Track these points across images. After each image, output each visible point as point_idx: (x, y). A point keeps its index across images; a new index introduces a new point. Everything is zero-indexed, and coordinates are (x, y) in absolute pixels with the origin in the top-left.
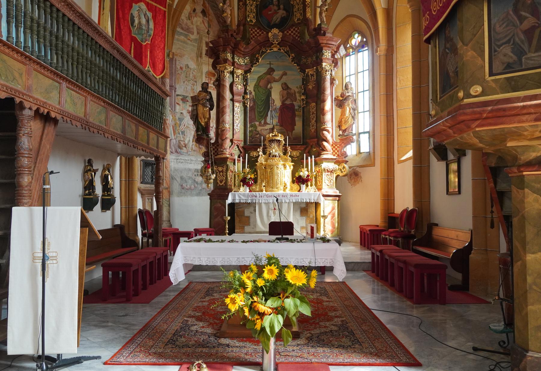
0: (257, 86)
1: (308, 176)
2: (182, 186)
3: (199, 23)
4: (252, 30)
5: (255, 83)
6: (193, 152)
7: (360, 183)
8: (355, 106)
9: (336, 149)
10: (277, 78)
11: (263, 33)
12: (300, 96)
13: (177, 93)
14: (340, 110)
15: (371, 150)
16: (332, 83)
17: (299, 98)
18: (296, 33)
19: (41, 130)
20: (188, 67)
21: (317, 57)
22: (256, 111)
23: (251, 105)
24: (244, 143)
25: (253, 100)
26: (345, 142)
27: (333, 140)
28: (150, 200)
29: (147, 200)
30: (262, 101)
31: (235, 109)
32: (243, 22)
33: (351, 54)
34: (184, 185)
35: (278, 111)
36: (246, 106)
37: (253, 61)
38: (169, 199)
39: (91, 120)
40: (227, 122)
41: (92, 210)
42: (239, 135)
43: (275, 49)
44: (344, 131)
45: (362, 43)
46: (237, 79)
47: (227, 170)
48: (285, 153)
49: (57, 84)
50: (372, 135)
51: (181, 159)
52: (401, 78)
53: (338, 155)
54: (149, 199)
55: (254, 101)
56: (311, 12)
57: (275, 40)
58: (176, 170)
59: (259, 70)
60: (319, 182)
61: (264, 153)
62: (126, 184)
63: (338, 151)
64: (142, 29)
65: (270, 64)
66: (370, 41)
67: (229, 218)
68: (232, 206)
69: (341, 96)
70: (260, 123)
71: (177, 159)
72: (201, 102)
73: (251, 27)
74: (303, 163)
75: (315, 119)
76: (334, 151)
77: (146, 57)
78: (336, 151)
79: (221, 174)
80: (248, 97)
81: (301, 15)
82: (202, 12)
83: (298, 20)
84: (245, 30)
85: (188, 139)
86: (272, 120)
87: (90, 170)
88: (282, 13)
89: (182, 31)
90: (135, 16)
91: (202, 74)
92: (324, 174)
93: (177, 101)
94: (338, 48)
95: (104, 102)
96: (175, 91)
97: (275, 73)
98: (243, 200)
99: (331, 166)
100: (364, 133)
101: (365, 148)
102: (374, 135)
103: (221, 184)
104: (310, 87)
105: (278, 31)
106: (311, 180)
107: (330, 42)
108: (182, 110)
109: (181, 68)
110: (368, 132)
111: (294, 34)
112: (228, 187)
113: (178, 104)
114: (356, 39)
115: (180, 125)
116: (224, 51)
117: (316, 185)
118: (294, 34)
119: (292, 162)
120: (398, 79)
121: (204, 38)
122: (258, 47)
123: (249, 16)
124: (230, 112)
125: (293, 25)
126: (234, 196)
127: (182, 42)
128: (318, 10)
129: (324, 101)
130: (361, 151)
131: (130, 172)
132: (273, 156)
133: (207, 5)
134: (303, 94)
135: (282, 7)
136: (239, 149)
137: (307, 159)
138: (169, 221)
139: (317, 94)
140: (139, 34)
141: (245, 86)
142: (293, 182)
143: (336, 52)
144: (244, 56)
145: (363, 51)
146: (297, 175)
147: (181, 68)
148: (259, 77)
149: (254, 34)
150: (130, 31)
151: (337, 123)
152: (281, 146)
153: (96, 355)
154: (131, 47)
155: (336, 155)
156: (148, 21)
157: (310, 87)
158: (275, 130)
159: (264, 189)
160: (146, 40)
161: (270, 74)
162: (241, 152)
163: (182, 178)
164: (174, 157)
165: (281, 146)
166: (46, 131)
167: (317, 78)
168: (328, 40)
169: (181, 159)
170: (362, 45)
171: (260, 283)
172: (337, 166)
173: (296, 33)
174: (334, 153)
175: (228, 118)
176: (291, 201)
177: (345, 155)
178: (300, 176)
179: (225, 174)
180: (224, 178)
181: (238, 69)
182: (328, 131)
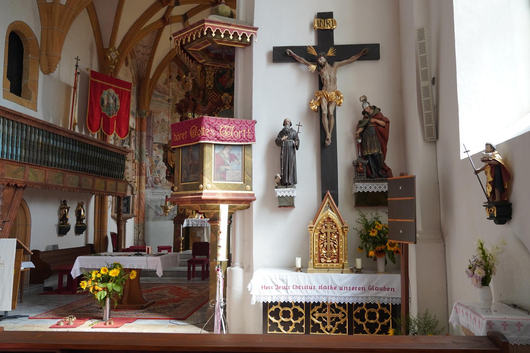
2: (156, 213)
3: (174, 86)
13: (154, 141)
19: (13, 193)
34: (159, 212)
39: (49, 182)
41: (65, 234)
49: (22, 168)
58: (151, 201)
62: (99, 214)
64: (110, 107)
67: (183, 238)
68: (187, 228)
77: (113, 125)
82: (176, 78)
85: (163, 176)
87: (64, 208)
89: (159, 94)
93: (154, 148)
95: (61, 170)
96: (152, 140)
108: (158, 154)
109: (158, 122)
112: (186, 214)
116: (186, 111)
121: (178, 98)
126: (188, 221)
133: (182, 72)
138: (144, 240)
147: (158, 122)
150: (101, 109)
153: (26, 315)
154: (100, 123)
156: (115, 101)
160: (113, 114)
163: (156, 207)
164: (150, 191)
166: (16, 193)
171: (99, 276)
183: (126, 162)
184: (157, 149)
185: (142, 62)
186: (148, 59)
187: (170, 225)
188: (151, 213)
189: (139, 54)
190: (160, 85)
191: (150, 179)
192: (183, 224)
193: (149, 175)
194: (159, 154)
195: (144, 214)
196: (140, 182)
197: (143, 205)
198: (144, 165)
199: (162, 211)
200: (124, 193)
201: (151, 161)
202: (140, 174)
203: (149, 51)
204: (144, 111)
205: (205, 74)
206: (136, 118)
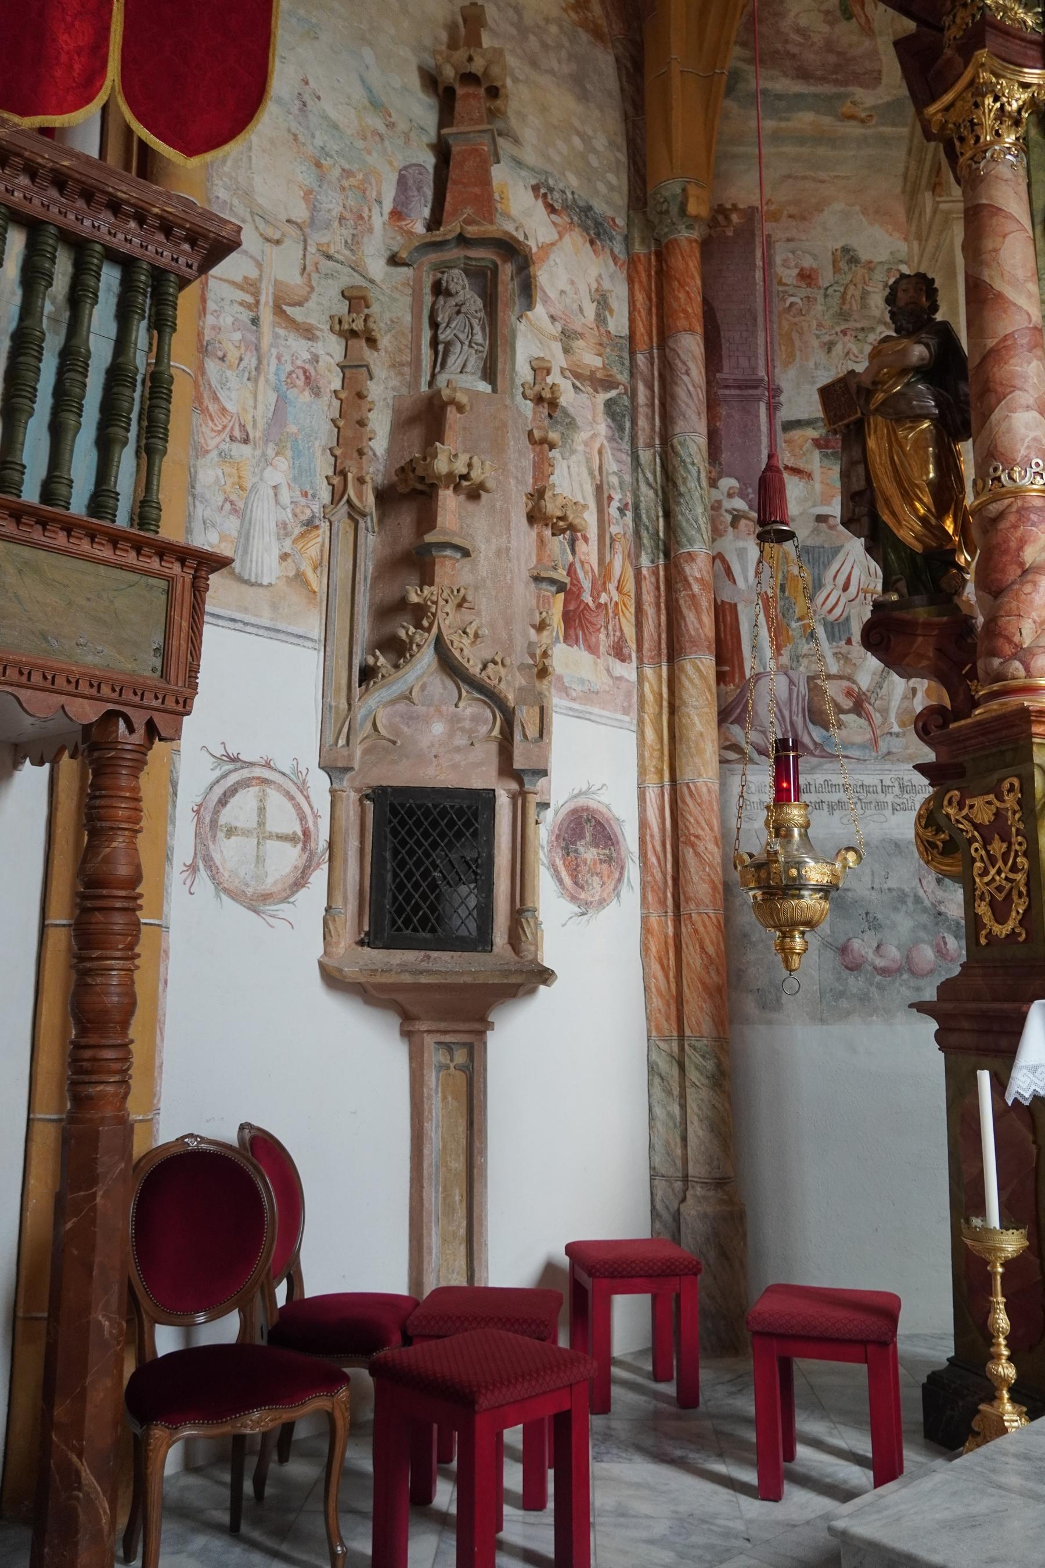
2: (844, 950)
13: (785, 414)
20: (854, 260)
28: (460, 1057)
29: (434, 1056)
34: (863, 946)
51: (829, 786)
54: (449, 1047)
79: (998, 847)
96: (773, 408)
103: (1002, 931)
109: (807, 277)
113: (796, 471)
115: (818, 585)
127: (801, 140)
169: (829, 786)
187: (917, 1051)
190: (802, 32)
206: (632, 263)
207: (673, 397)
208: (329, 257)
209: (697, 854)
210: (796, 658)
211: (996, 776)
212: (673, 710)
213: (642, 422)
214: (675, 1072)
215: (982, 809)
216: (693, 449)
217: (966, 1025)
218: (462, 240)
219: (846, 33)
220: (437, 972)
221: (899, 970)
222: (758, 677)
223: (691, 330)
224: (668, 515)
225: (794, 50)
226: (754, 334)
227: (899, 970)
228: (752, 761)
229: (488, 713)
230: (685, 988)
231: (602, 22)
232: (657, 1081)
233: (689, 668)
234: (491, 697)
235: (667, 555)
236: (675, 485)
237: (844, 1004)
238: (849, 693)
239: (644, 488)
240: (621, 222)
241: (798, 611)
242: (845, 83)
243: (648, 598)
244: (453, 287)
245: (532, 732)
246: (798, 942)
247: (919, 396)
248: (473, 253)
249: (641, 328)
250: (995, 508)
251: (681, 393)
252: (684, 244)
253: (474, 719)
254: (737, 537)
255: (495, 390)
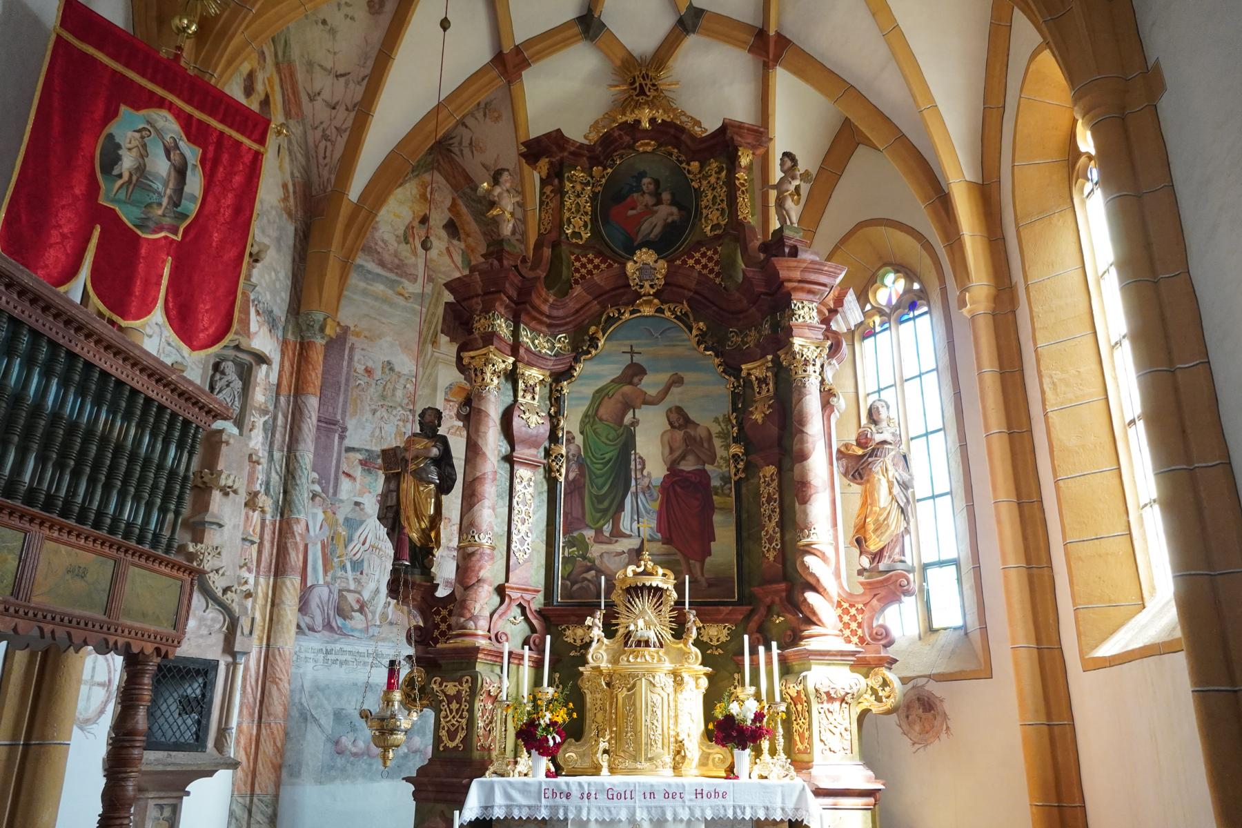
0: (589, 419)
1: (759, 716)
2: (337, 743)
4: (577, 259)
5: (585, 408)
6: (386, 628)
7: (943, 736)
8: (906, 476)
9: (854, 618)
10: (652, 392)
11: (610, 266)
12: (727, 447)
13: (348, 442)
14: (856, 488)
15: (973, 624)
16: (826, 405)
17: (725, 454)
18: (710, 265)
20: (392, 369)
21: (775, 326)
22: (587, 492)
23: (571, 476)
24: (546, 598)
25: (580, 462)
26: (882, 592)
27: (841, 587)
28: (167, 812)
30: (606, 464)
31: (518, 487)
32: (553, 239)
33: (878, 329)
34: (346, 741)
35: (656, 493)
36: (556, 479)
37: (581, 345)
38: (276, 797)
40: (484, 527)
42: (529, 572)
43: (647, 311)
44: (877, 556)
45: (909, 298)
46: (529, 396)
47: (473, 692)
48: (679, 632)
50: (973, 571)
51: (342, 651)
52: (1057, 375)
53: (862, 640)
54: (161, 807)
55: (581, 465)
56: (753, 206)
57: (647, 284)
58: (318, 688)
59: (597, 372)
60: (801, 736)
61: (609, 632)
63: (860, 625)
65: (632, 353)
66: (937, 283)
69: (859, 444)
70: (599, 531)
71: (327, 652)
72: (412, 467)
73: (577, 251)
74: (740, 669)
75: (776, 518)
76: (847, 625)
78: (854, 625)
79: (454, 706)
80: (564, 451)
81: (722, 214)
82: (446, 227)
83: (714, 228)
84: (556, 259)
85: (372, 586)
86: (639, 520)
88: (666, 212)
89: (379, 270)
90: (125, 144)
91: (435, 389)
92: (815, 707)
93: (344, 467)
94: (839, 301)
96: (342, 438)
97: (646, 379)
98: (520, 807)
99: (842, 678)
100: (941, 564)
101: (950, 610)
102: (977, 570)
103: (451, 745)
104: (758, 417)
105: (655, 257)
106: (771, 733)
107: (813, 277)
108: (361, 494)
109: (368, 371)
110: (956, 562)
111: (705, 267)
112: (476, 755)
113: (348, 475)
114: (891, 288)
115: (350, 540)
116: (487, 310)
117: (789, 751)
118: (705, 267)
119: (704, 663)
120: (1046, 380)
122: (595, 306)
123: (569, 222)
124: (499, 496)
125: (700, 244)
126: (489, 792)
127: (376, 298)
128: (773, 194)
129: (803, 457)
130: (935, 626)
131: (41, 705)
132: (639, 644)
133: (464, 210)
134: (736, 440)
135: (666, 196)
136: (527, 619)
137: (753, 652)
139: (780, 438)
140: (129, 201)
141: (554, 419)
142: (709, 735)
143: (833, 312)
144: (552, 327)
145: (914, 318)
146: (719, 714)
148: (597, 392)
149: (583, 271)
150: (93, 188)
151: (852, 532)
152: (666, 609)
155: (855, 639)
156: (181, 172)
157: (758, 417)
158: (646, 555)
159: (604, 761)
161: (631, 383)
162: (533, 629)
163: (338, 716)
164: (316, 645)
165: (666, 609)
167: (776, 389)
168: (805, 270)
169: (342, 651)
170: (910, 303)
172: (861, 677)
173: (710, 265)
174: (847, 632)
175: (489, 514)
176: (698, 814)
177: (883, 637)
178: (730, 718)
179: (465, 706)
180: (464, 721)
181: (530, 364)
182: (823, 557)
183: (216, 495)
184: (358, 472)
185: (325, 137)
186: (349, 123)
188: (314, 747)
189: (319, 103)
191: (321, 594)
192: (460, 805)
193: (316, 575)
194: (364, 492)
195: (280, 752)
196: (275, 603)
197: (277, 707)
198: (299, 529)
199: (366, 733)
200: (166, 629)
201: (330, 521)
202: (279, 569)
203: (357, 92)
204: (319, 317)
205: (560, 192)
206: (285, 343)
207: (300, 429)
208: (169, 344)
209: (278, 689)
210: (334, 578)
211: (459, 674)
212: (273, 605)
213: (278, 435)
214: (246, 816)
215: (451, 689)
216: (307, 461)
217: (430, 788)
218: (237, 348)
219: (404, 250)
220: (174, 764)
221: (363, 754)
222: (312, 587)
223: (315, 395)
224: (285, 492)
225: (379, 250)
226: (338, 395)
227: (363, 754)
228: (304, 634)
229: (221, 618)
230: (260, 762)
231: (293, 208)
232: (234, 821)
233: (288, 583)
234: (225, 609)
235: (282, 516)
236: (294, 478)
237: (333, 773)
238: (358, 601)
239: (273, 474)
240: (283, 319)
241: (338, 552)
242: (401, 276)
243: (267, 537)
244: (227, 371)
245: (246, 631)
246: (391, 755)
247: (431, 472)
248: (241, 355)
249: (285, 382)
250: (470, 550)
251: (305, 428)
252: (318, 345)
253: (213, 619)
254: (313, 506)
255: (241, 434)
